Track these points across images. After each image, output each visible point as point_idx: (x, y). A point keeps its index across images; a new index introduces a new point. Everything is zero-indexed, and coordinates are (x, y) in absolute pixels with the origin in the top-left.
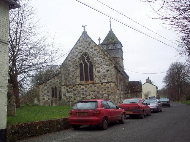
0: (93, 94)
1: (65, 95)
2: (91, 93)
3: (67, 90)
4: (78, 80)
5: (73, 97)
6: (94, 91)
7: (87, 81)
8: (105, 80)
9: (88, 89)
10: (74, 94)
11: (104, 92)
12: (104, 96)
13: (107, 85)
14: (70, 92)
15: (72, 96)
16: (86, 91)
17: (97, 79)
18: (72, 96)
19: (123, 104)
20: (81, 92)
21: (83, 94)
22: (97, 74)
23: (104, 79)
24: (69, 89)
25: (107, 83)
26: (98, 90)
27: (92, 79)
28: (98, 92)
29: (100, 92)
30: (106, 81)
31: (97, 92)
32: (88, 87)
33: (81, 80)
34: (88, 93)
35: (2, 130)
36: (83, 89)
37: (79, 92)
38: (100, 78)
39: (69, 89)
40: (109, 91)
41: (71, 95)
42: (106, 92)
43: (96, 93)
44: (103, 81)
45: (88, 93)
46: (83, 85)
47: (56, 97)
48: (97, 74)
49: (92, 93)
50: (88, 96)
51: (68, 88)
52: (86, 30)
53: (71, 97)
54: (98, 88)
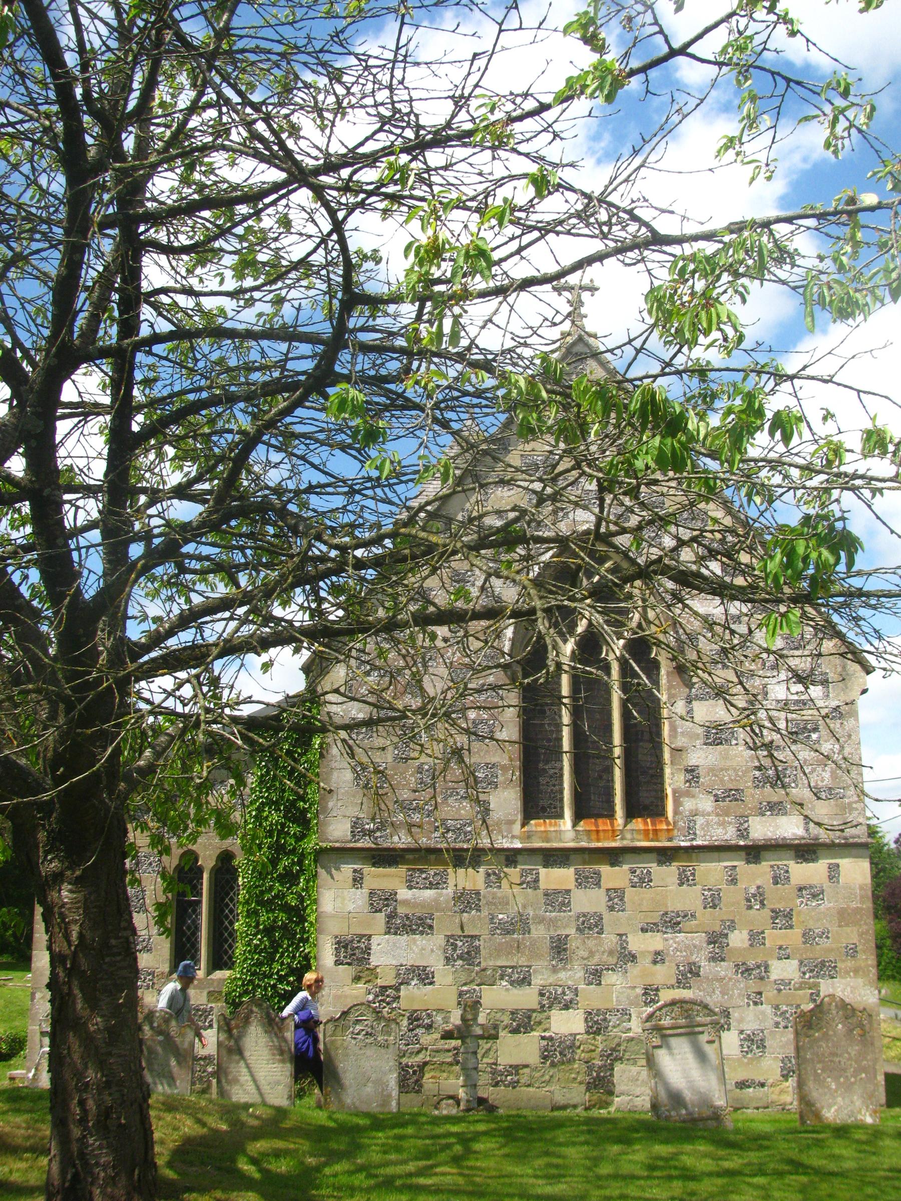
0: (658, 957)
1: (353, 952)
2: (643, 944)
3: (383, 901)
4: (506, 801)
5: (450, 979)
6: (672, 922)
7: (603, 824)
8: (783, 820)
9: (616, 898)
10: (461, 950)
11: (773, 937)
12: (774, 975)
13: (802, 872)
14: (418, 924)
15: (436, 963)
16: (591, 924)
17: (706, 803)
18: (436, 963)
19: (135, 915)
20: (539, 932)
21: (559, 949)
22: (700, 756)
23: (775, 808)
24: (404, 894)
25: (805, 851)
26: (709, 919)
27: (645, 800)
28: (716, 939)
29: (738, 939)
30: (790, 827)
31: (699, 938)
32: (606, 883)
33: (537, 803)
34: (609, 939)
35: (263, 1195)
36: (557, 899)
37: (520, 924)
38: (733, 795)
39: (404, 894)
40: (825, 934)
41: (424, 950)
42: (794, 936)
43: (687, 943)
44: (762, 829)
45: (609, 939)
46: (554, 857)
47: (220, 960)
48: (700, 756)
49: (655, 942)
50: (610, 978)
51: (390, 879)
52: (590, 325)
53: (425, 976)
54: (713, 902)
